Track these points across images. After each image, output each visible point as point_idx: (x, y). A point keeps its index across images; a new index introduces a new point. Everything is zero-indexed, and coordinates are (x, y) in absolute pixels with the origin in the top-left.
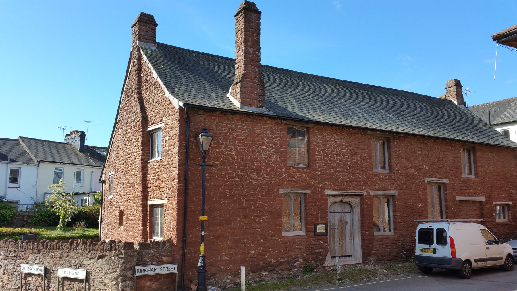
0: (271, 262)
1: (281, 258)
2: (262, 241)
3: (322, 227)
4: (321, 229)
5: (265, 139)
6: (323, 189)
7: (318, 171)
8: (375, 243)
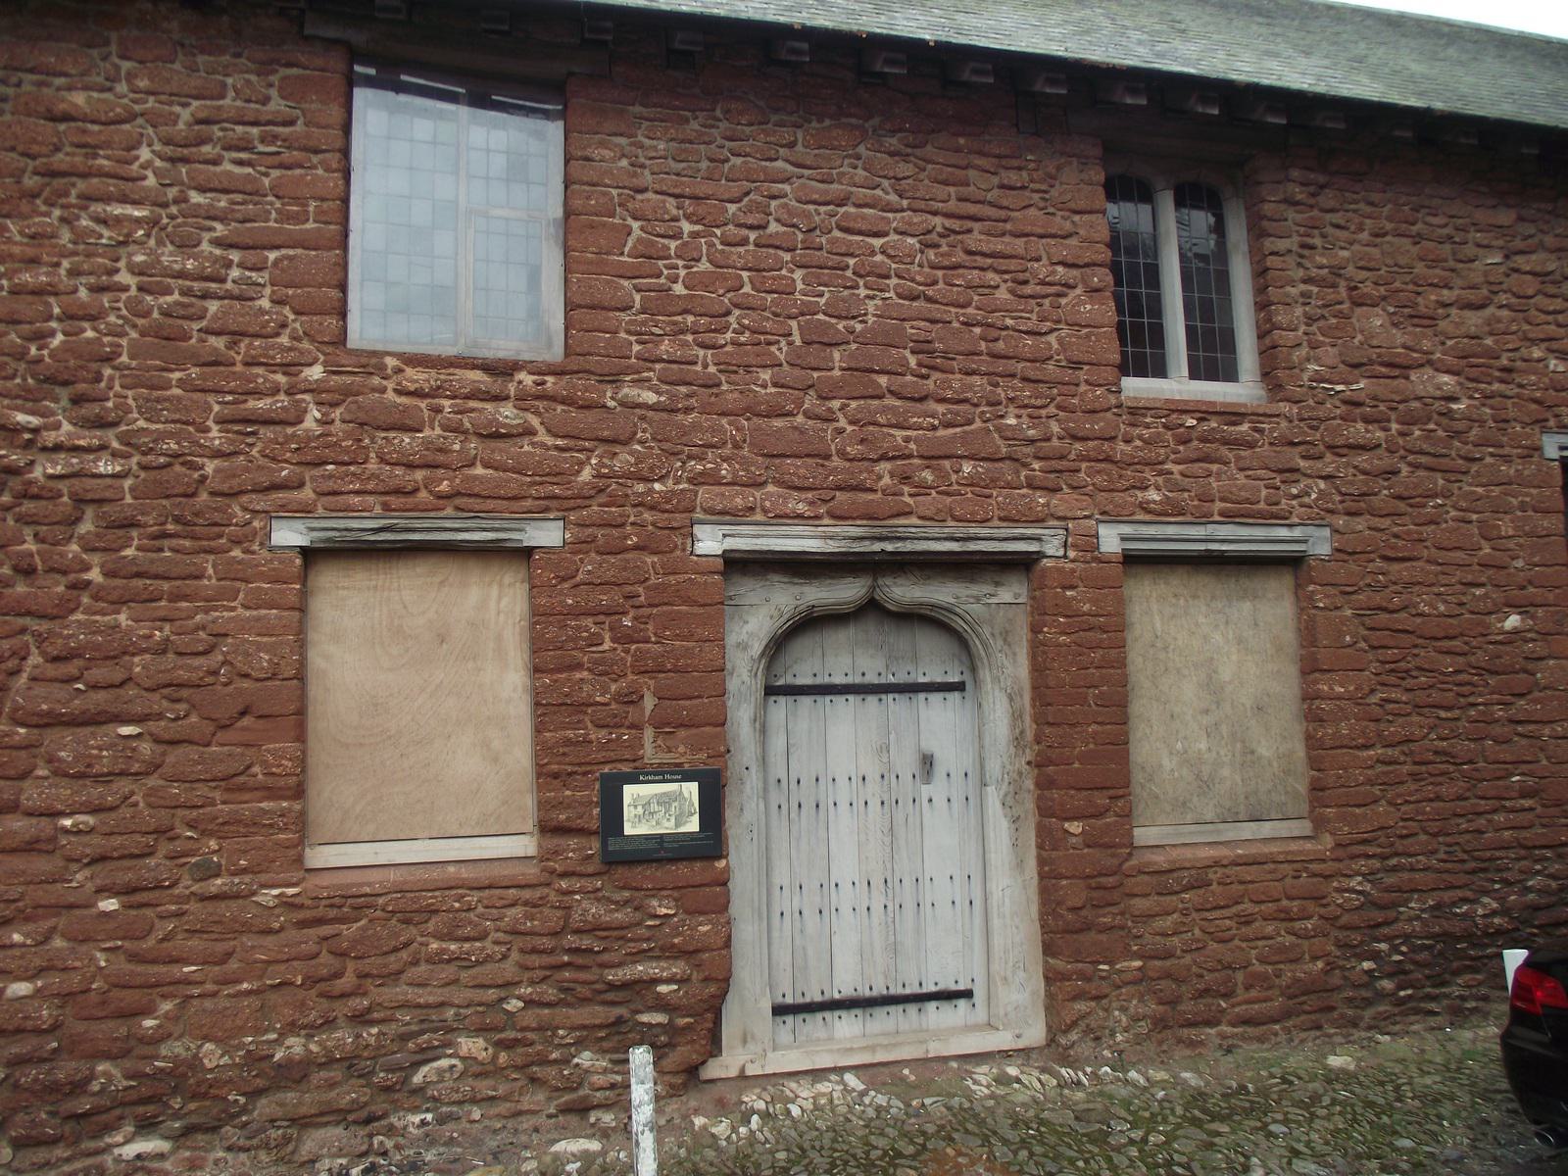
0: (195, 1063)
1: (292, 1028)
2: (110, 904)
3: (665, 801)
4: (657, 809)
5: (145, 154)
6: (680, 517)
7: (639, 382)
8: (1140, 904)
